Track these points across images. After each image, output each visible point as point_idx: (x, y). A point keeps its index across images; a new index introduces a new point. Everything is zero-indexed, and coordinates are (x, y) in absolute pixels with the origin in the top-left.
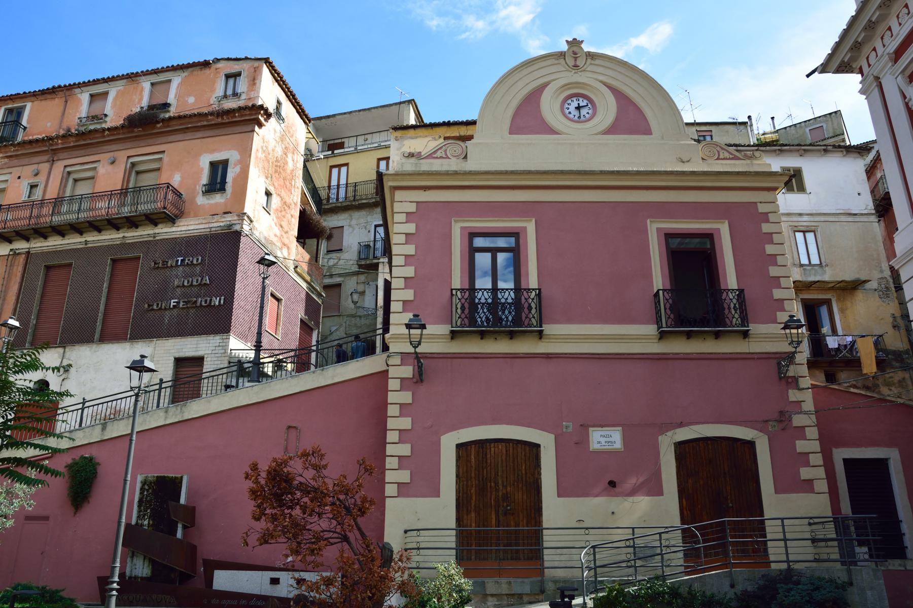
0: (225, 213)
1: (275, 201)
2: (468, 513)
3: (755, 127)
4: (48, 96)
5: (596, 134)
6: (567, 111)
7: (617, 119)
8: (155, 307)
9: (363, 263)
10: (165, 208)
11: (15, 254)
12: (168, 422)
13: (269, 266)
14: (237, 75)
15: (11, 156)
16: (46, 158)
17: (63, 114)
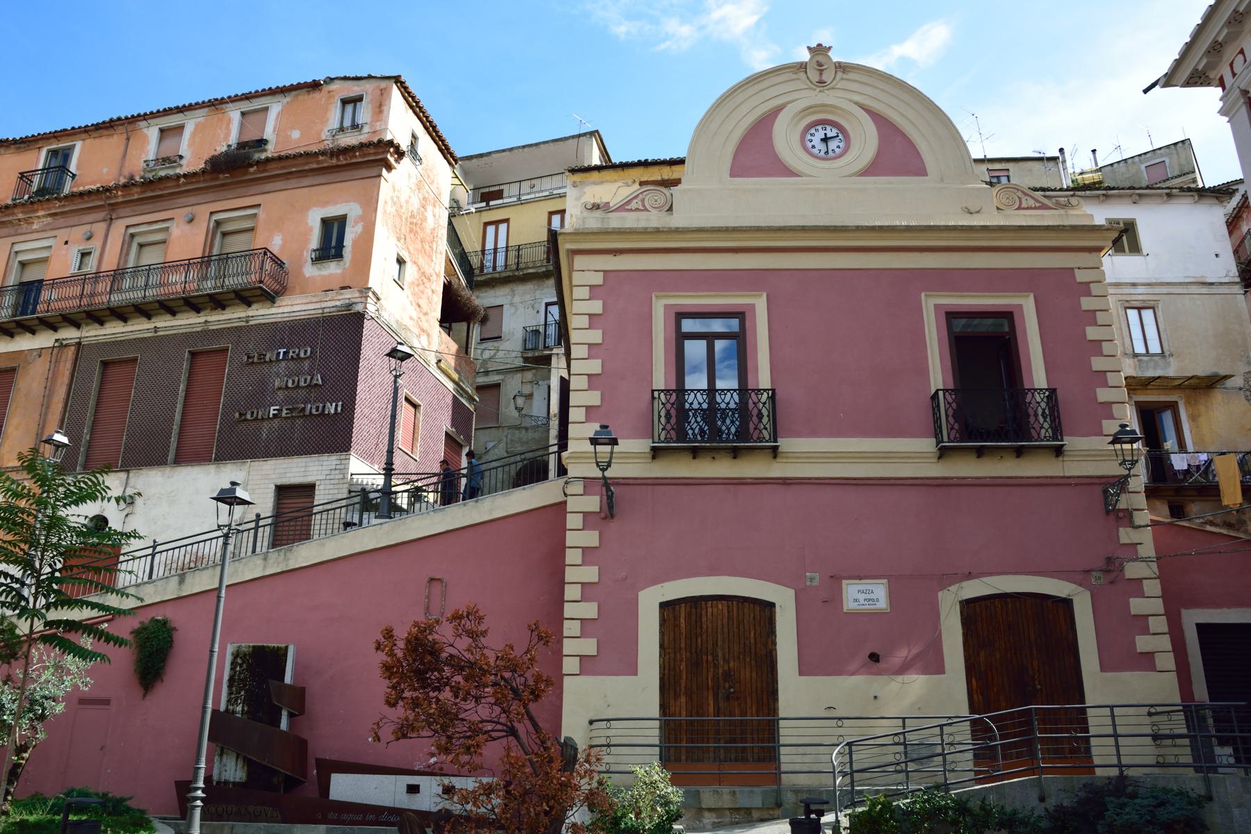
2: (676, 697)
3: (1069, 164)
4: (105, 132)
6: (810, 145)
7: (879, 155)
8: (249, 417)
9: (530, 355)
10: (261, 282)
11: (62, 345)
13: (402, 359)
16: (101, 215)
17: (124, 156)
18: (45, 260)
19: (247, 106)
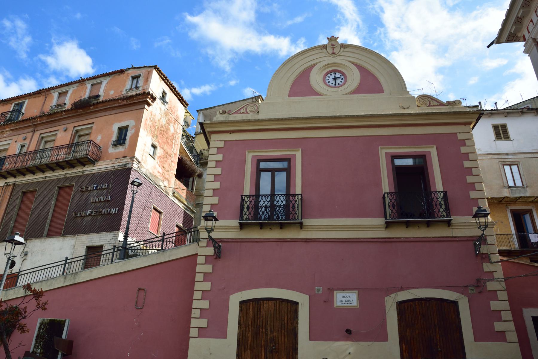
0: (123, 157)
1: (159, 151)
2: (245, 350)
4: (38, 95)
5: (346, 94)
7: (360, 84)
8: (78, 215)
11: (8, 185)
12: (65, 285)
13: (138, 186)
14: (138, 77)
15: (13, 130)
16: (31, 129)
17: (43, 105)
18: (6, 150)
19: (93, 82)
